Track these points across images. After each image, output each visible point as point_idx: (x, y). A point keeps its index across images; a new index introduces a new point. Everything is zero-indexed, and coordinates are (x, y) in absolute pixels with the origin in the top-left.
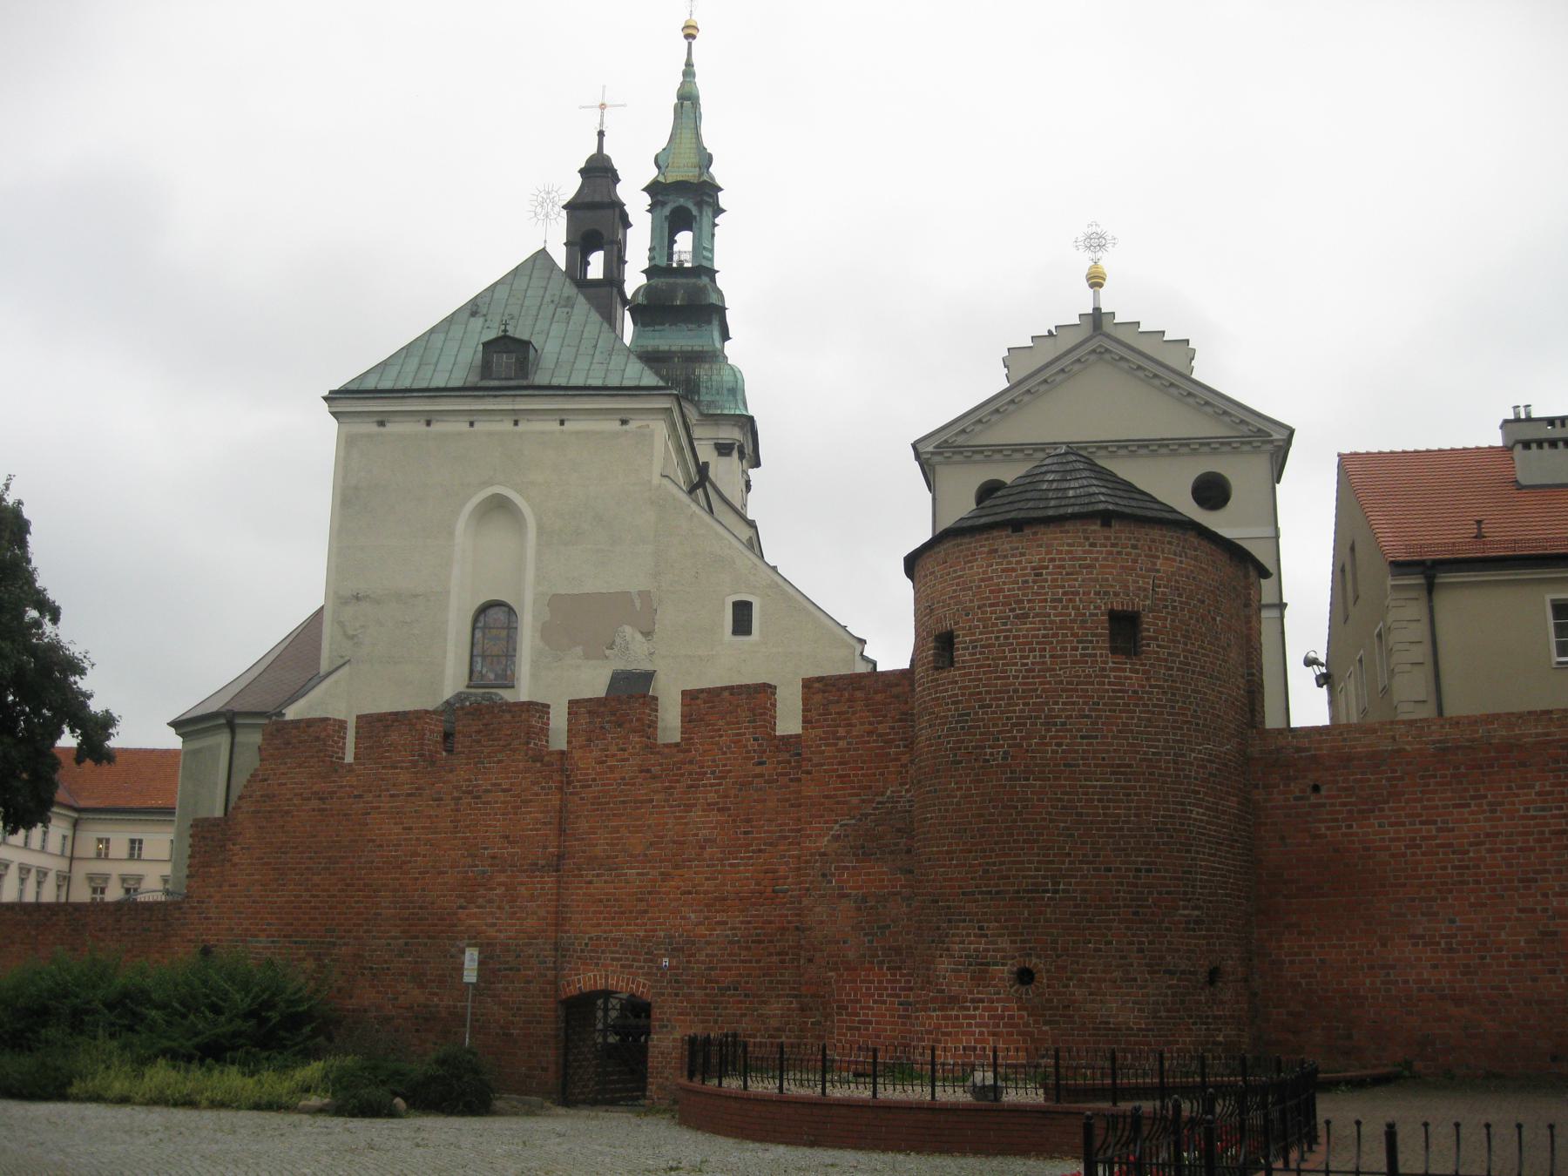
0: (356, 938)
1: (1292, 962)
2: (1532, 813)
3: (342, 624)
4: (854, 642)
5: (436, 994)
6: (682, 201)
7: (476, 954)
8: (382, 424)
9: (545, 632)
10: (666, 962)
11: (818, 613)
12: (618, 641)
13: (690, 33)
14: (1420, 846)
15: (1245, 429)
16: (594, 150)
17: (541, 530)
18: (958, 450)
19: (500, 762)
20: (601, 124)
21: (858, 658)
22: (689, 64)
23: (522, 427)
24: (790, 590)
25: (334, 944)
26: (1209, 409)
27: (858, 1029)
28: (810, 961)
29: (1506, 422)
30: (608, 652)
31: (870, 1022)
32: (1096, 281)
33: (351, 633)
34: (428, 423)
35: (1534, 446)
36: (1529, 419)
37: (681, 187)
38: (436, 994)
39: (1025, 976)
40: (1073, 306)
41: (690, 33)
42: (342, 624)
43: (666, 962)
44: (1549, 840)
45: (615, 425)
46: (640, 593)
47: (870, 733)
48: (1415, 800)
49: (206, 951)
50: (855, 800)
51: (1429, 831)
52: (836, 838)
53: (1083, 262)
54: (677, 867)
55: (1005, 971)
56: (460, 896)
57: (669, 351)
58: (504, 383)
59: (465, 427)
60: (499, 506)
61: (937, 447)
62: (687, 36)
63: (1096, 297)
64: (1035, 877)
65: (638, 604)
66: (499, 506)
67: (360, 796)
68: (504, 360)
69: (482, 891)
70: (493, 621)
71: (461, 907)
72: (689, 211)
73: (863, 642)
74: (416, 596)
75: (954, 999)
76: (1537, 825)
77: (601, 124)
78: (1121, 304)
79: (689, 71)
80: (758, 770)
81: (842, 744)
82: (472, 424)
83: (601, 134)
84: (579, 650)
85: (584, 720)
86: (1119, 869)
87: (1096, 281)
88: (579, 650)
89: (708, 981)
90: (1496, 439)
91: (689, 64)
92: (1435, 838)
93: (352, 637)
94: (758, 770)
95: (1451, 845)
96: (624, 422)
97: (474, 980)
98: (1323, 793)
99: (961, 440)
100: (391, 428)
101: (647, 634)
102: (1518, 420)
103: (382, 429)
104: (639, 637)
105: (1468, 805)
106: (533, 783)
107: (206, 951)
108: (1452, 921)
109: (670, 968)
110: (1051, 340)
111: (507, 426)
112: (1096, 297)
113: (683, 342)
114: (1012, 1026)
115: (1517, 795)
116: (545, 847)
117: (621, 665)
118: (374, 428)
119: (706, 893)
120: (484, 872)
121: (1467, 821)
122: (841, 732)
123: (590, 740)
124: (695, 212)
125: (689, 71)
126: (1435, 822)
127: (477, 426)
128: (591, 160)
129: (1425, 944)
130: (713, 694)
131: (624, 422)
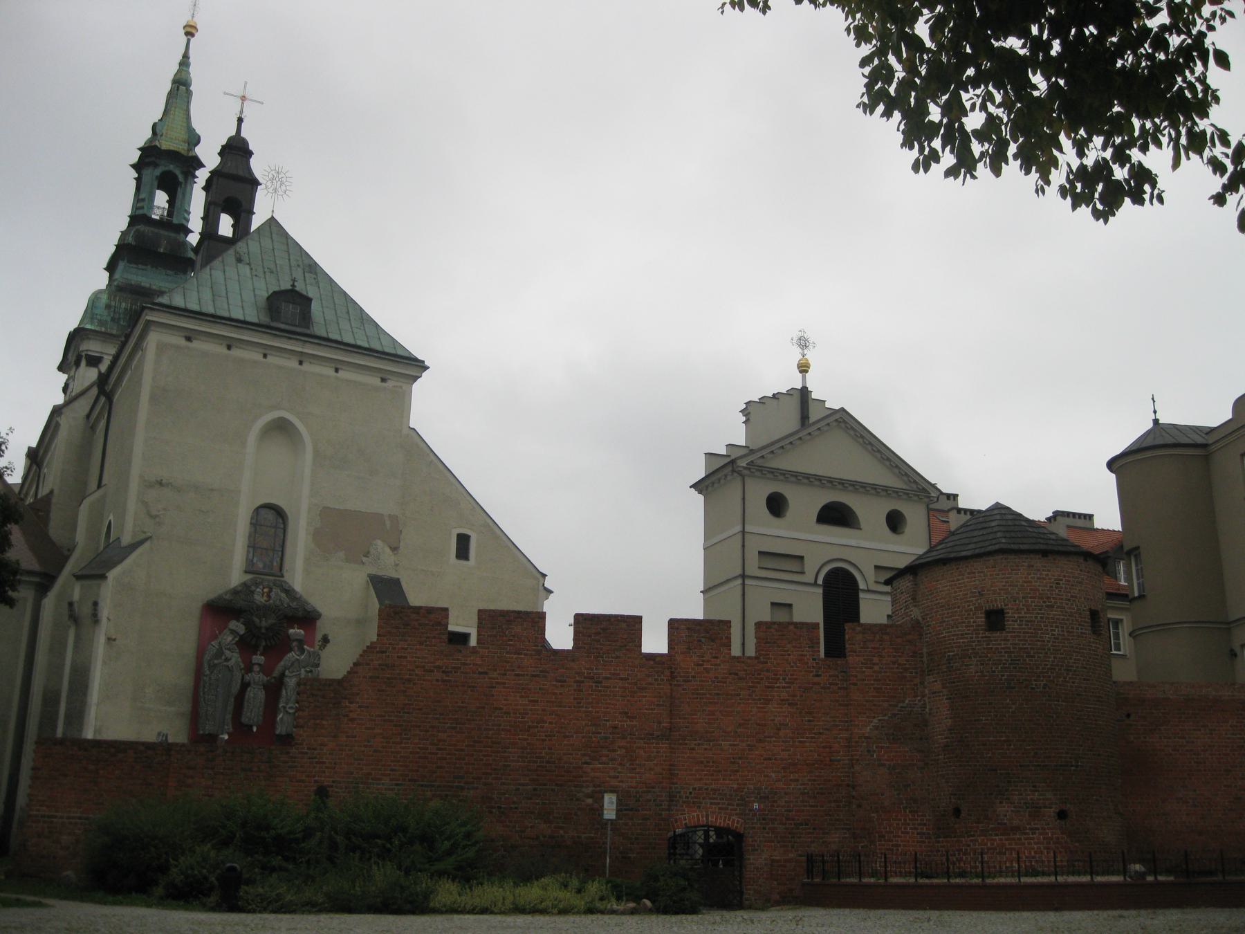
0: (485, 784)
3: (146, 504)
4: (539, 576)
5: (561, 828)
6: (171, 167)
7: (614, 798)
8: (189, 339)
9: (317, 535)
10: (756, 806)
12: (372, 551)
13: (190, 31)
15: (914, 486)
16: (233, 133)
17: (317, 453)
19: (617, 657)
20: (241, 112)
22: (186, 56)
23: (341, 374)
25: (462, 788)
26: (896, 471)
28: (859, 806)
30: (364, 559)
32: (803, 368)
33: (154, 513)
34: (229, 347)
37: (173, 155)
38: (561, 828)
39: (1062, 815)
40: (785, 380)
41: (190, 31)
42: (146, 504)
43: (756, 806)
45: (376, 381)
46: (390, 516)
47: (894, 663)
49: (322, 792)
50: (886, 705)
52: (876, 728)
53: (796, 355)
54: (760, 741)
55: (1052, 811)
56: (584, 755)
57: (150, 289)
58: (287, 327)
59: (260, 357)
60: (281, 428)
62: (187, 34)
63: (804, 379)
65: (388, 523)
66: (281, 428)
67: (486, 673)
68: (289, 309)
69: (605, 752)
70: (271, 521)
71: (586, 763)
72: (175, 177)
73: (544, 576)
74: (212, 490)
75: (1016, 829)
77: (241, 112)
79: (185, 62)
80: (816, 679)
81: (876, 668)
82: (265, 356)
83: (240, 120)
84: (342, 554)
87: (803, 368)
88: (342, 554)
89: (787, 819)
91: (186, 56)
93: (153, 517)
94: (816, 679)
96: (383, 380)
97: (614, 817)
99: (760, 462)
100: (196, 344)
101: (395, 549)
103: (188, 344)
104: (388, 550)
106: (648, 676)
107: (322, 792)
109: (759, 810)
110: (775, 402)
111: (293, 364)
112: (804, 379)
113: (162, 284)
116: (660, 723)
117: (374, 571)
118: (183, 342)
119: (782, 760)
120: (606, 738)
122: (876, 660)
123: (689, 648)
124: (181, 178)
125: (185, 62)
127: (270, 359)
128: (230, 139)
130: (582, 615)
131: (383, 380)
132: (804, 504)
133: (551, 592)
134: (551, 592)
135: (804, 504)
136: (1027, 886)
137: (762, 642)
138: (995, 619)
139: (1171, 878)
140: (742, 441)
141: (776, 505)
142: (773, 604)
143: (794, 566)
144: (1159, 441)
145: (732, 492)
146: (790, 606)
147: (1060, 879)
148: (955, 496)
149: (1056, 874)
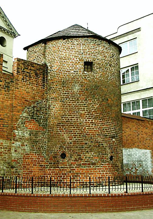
64: (113, 132)
138: (88, 65)
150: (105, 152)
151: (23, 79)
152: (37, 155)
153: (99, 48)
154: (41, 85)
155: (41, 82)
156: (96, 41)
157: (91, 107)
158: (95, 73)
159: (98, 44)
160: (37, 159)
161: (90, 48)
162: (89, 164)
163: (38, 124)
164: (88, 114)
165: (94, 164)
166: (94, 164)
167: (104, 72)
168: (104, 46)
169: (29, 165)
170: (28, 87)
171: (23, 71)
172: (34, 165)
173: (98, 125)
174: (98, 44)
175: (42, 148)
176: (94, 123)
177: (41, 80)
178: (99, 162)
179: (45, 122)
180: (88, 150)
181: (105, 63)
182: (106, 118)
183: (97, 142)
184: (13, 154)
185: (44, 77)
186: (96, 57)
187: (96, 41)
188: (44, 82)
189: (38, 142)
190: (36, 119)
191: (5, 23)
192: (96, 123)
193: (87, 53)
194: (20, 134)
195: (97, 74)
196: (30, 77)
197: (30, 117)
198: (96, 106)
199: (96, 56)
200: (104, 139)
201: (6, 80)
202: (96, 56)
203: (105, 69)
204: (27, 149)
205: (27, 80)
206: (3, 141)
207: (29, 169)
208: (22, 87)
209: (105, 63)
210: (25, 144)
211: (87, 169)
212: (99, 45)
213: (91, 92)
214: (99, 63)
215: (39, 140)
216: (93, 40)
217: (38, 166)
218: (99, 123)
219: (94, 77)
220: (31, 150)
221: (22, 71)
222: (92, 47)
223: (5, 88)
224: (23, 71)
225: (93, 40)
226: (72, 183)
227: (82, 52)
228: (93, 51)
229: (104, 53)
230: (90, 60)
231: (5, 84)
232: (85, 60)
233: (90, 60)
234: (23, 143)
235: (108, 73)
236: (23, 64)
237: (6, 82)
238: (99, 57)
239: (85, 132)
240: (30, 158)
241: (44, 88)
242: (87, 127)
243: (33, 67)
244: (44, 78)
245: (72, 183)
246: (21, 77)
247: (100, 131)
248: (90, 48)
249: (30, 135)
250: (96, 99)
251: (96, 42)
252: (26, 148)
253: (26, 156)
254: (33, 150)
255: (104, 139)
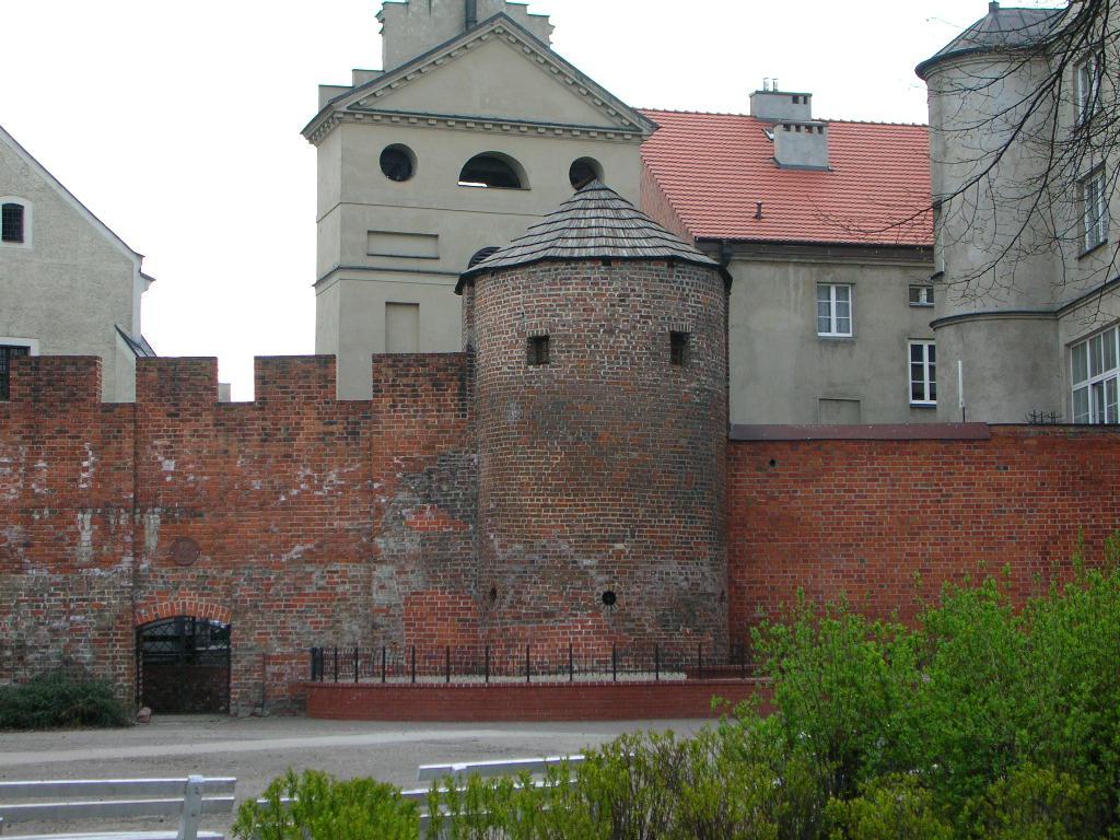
1: (751, 588)
2: (919, 488)
11: (96, 224)
14: (843, 508)
18: (370, 113)
21: (136, 274)
24: (77, 207)
27: (424, 641)
29: (757, 92)
31: (435, 636)
35: (793, 128)
36: (775, 93)
44: (929, 507)
48: (841, 475)
51: (849, 497)
61: (349, 108)
64: (618, 526)
73: (141, 257)
76: (922, 496)
78: (1053, 324)
85: (153, 375)
86: (674, 521)
90: (744, 108)
92: (854, 502)
95: (864, 508)
98: (777, 466)
102: (766, 92)
105: (877, 480)
108: (862, 561)
114: (600, 633)
115: (911, 475)
121: (875, 491)
126: (854, 491)
129: (844, 576)
132: (442, 156)
133: (152, 280)
134: (152, 280)
135: (442, 156)
136: (626, 685)
137: (261, 381)
138: (539, 347)
139: (682, 677)
140: (376, 63)
141: (397, 163)
142: (387, 304)
143: (423, 248)
144: (995, 41)
145: (338, 140)
146: (418, 305)
147: (455, 680)
148: (806, 98)
149: (448, 673)
150: (585, 583)
151: (394, 406)
152: (450, 593)
153: (569, 289)
154: (453, 410)
155: (452, 401)
156: (557, 269)
157: (544, 463)
158: (553, 367)
159: (565, 279)
160: (449, 603)
161: (542, 296)
162: (538, 616)
163: (446, 514)
164: (536, 484)
165: (549, 615)
166: (549, 615)
167: (583, 357)
168: (584, 279)
169: (425, 619)
170: (410, 422)
171: (393, 386)
172: (438, 619)
173: (561, 511)
174: (565, 279)
175: (466, 576)
176: (551, 506)
177: (454, 395)
178: (562, 609)
179: (470, 506)
180: (535, 578)
181: (586, 330)
182: (589, 489)
183: (560, 557)
184: (374, 595)
185: (463, 384)
186: (557, 319)
187: (557, 269)
188: (465, 400)
189: (450, 560)
190: (438, 501)
191: (589, 100)
192: (556, 505)
193: (534, 311)
194: (392, 545)
195: (562, 365)
196: (417, 396)
197: (418, 499)
198: (557, 459)
199: (558, 315)
200: (581, 546)
201: (347, 418)
202: (558, 315)
203: (589, 346)
204: (417, 580)
205: (408, 406)
206: (346, 566)
207: (424, 630)
208: (393, 427)
209: (586, 330)
210: (409, 568)
211: (532, 629)
212: (569, 279)
213: (543, 423)
214: (566, 336)
215: (453, 555)
216: (549, 271)
217: (453, 620)
218: (566, 506)
219: (552, 377)
220: (428, 582)
221: (389, 386)
222: (545, 290)
223: (346, 438)
224: (393, 386)
225: (549, 271)
226: (575, 656)
227: (523, 310)
228: (548, 304)
229: (585, 300)
230: (542, 331)
231: (345, 428)
232: (530, 333)
233: (542, 331)
234: (403, 567)
235: (598, 358)
236: (389, 366)
237: (348, 423)
238: (566, 316)
239: (530, 532)
240: (427, 604)
241: (464, 416)
242: (534, 519)
243: (424, 366)
244: (462, 388)
245: (575, 656)
246: (386, 402)
247: (567, 526)
248: (542, 296)
249: (425, 545)
250: (556, 438)
251: (559, 274)
252: (411, 577)
253: (412, 599)
254: (435, 582)
255: (581, 546)
